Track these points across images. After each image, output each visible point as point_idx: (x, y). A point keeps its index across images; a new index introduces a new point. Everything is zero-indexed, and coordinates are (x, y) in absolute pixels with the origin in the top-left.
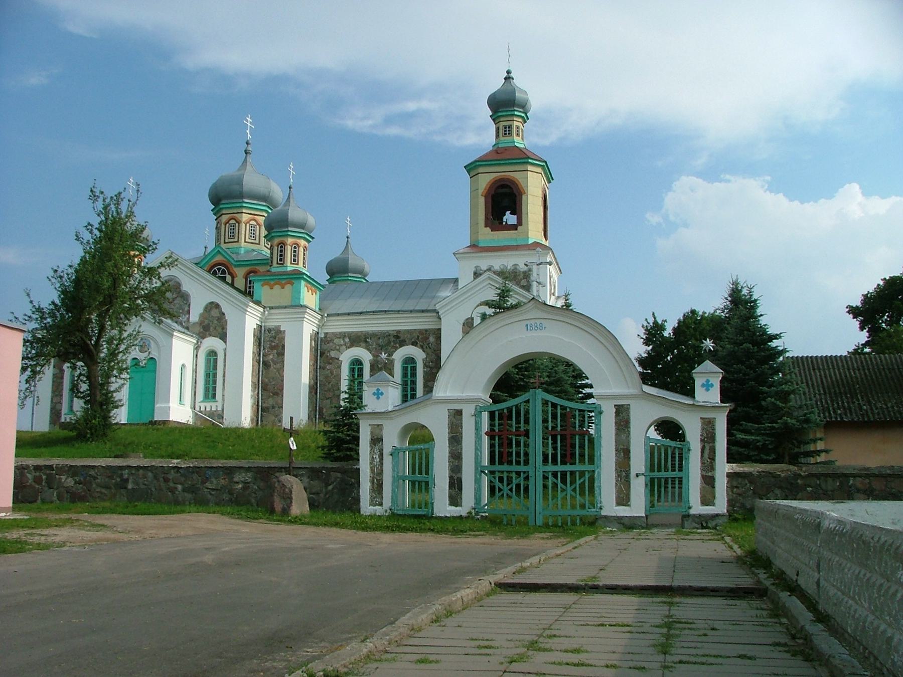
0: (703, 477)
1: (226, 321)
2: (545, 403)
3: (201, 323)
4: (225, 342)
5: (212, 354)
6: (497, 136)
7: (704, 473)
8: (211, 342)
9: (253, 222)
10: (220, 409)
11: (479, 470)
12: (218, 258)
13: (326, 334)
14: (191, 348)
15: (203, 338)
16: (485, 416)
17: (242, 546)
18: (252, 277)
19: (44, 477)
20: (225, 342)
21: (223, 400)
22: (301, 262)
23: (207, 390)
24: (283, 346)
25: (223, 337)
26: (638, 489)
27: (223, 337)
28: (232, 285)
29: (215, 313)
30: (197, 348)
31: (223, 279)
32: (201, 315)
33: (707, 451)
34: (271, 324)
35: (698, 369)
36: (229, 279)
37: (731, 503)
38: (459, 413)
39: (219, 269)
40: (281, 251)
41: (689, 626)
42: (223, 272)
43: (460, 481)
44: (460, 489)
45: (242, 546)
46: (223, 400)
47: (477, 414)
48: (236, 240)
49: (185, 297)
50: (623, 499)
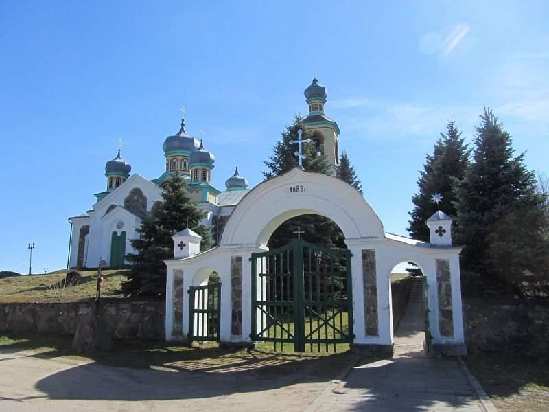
0: (441, 311)
6: (310, 111)
13: (221, 217)
33: (443, 288)
37: (467, 333)
38: (239, 259)
43: (240, 313)
44: (240, 320)
47: (253, 259)
49: (144, 199)
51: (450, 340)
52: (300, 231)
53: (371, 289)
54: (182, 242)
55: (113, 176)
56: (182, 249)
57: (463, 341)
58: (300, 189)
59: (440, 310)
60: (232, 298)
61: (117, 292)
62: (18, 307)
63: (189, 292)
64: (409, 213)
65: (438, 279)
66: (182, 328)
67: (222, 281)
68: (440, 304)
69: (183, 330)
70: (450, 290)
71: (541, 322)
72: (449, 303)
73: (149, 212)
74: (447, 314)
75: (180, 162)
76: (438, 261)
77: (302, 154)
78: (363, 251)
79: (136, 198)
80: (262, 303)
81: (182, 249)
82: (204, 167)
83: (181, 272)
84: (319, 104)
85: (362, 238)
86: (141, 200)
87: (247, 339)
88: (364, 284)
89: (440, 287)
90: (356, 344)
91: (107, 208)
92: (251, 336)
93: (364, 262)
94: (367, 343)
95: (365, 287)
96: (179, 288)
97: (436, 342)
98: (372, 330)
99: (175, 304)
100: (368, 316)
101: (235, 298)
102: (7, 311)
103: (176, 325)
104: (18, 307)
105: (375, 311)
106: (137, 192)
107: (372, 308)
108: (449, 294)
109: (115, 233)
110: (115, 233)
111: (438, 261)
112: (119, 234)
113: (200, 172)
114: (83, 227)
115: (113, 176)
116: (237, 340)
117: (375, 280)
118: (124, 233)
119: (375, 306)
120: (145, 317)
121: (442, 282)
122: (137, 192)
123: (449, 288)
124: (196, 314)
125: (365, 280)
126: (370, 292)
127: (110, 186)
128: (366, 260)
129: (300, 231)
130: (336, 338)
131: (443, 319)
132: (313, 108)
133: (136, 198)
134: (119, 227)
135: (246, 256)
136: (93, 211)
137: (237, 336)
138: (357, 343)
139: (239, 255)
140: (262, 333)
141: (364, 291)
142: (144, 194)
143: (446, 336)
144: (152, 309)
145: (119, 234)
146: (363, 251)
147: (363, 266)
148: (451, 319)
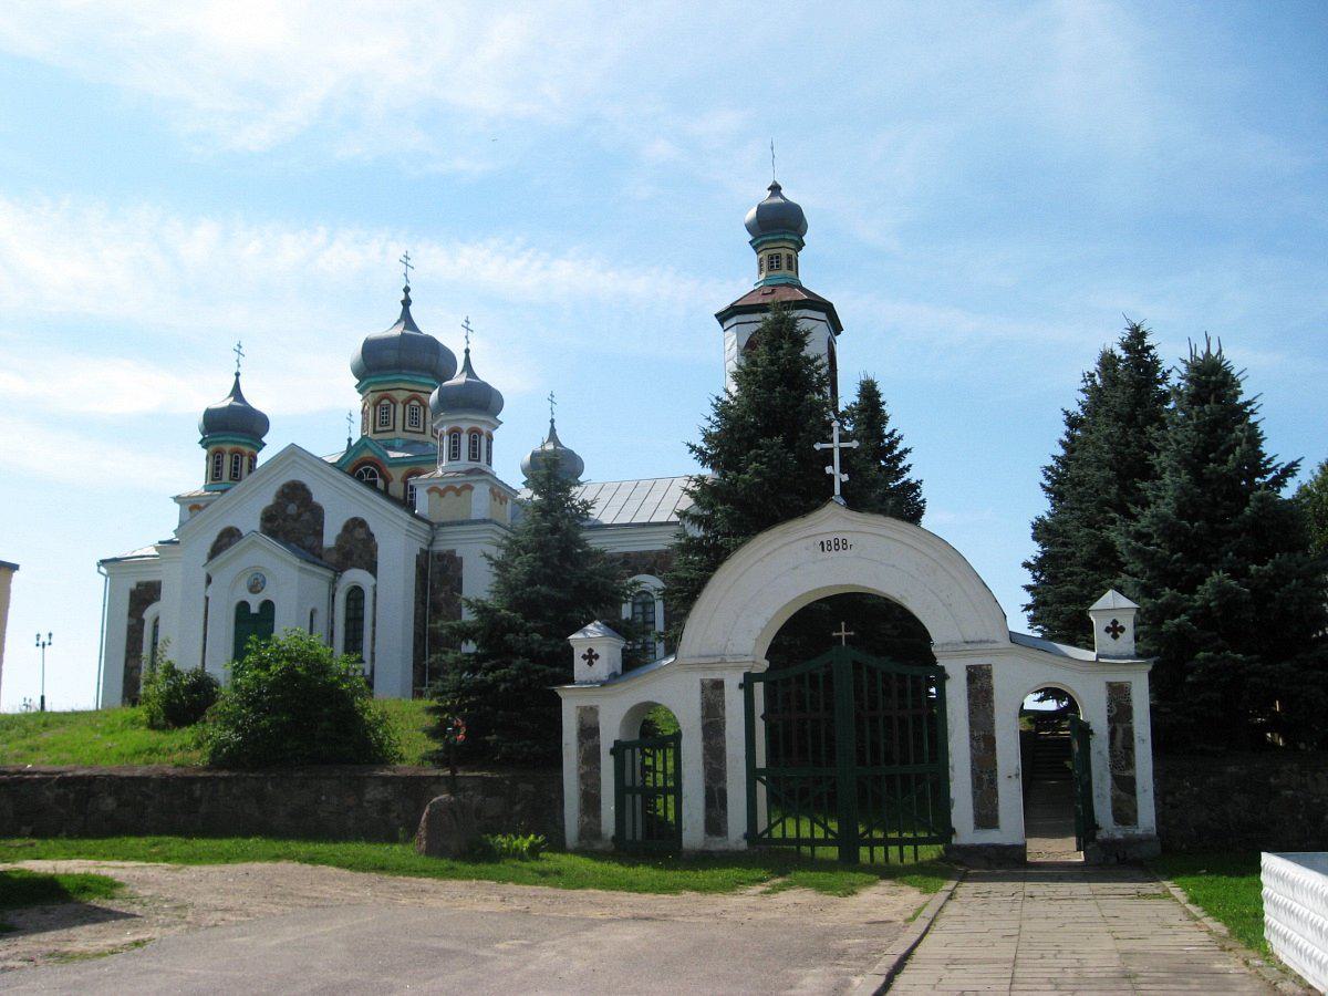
0: (1115, 778)
1: (376, 546)
2: (857, 666)
3: (339, 547)
4: (375, 576)
5: (356, 595)
7: (1117, 772)
8: (356, 576)
9: (385, 402)
10: (368, 672)
11: (753, 774)
12: (366, 454)
14: (325, 589)
15: (342, 571)
16: (759, 688)
17: (422, 380)
18: (412, 481)
19: (72, 796)
20: (375, 576)
21: (373, 660)
22: (484, 457)
23: (347, 641)
24: (460, 580)
25: (372, 568)
26: (1010, 794)
27: (372, 568)
28: (385, 494)
29: (359, 533)
30: (333, 584)
31: (372, 485)
32: (339, 538)
33: (1120, 735)
34: (442, 546)
35: (1098, 605)
36: (380, 483)
37: (1161, 817)
38: (718, 685)
39: (366, 470)
40: (455, 442)
41: (979, 976)
42: (373, 474)
43: (723, 794)
45: (422, 380)
46: (373, 660)
48: (391, 427)
49: (317, 513)
50: (986, 816)
51: (1130, 830)
52: (840, 637)
53: (984, 741)
54: (590, 651)
55: (242, 447)
56: (590, 664)
57: (1155, 832)
58: (840, 545)
59: (1113, 776)
60: (705, 764)
61: (199, 770)
62: (222, 786)
63: (612, 752)
64: (350, 440)
65: (1110, 720)
66: (600, 825)
67: (683, 727)
68: (1114, 766)
69: (603, 829)
70: (1132, 739)
71: (1291, 792)
72: (1130, 764)
73: (330, 550)
74: (1125, 785)
75: (400, 409)
76: (1110, 685)
77: (831, 477)
78: (968, 667)
79: (292, 509)
80: (761, 771)
81: (590, 664)
82: (452, 425)
83: (593, 711)
84: (784, 252)
85: (967, 642)
86: (307, 516)
87: (737, 842)
88: (971, 731)
89: (1113, 734)
90: (958, 846)
91: (212, 536)
92: (746, 836)
93: (969, 690)
94: (978, 842)
95: (972, 738)
96: (590, 743)
97: (1106, 836)
98: (986, 816)
99: (582, 777)
100: (979, 792)
101: (711, 763)
102: (198, 793)
103: (586, 820)
104: (222, 786)
105: (993, 782)
106: (295, 493)
107: (986, 777)
108: (1129, 748)
109: (243, 607)
110: (243, 607)
111: (1110, 685)
112: (254, 609)
113: (227, 459)
114: (139, 585)
115: (242, 447)
116: (717, 844)
117: (992, 724)
118: (268, 607)
119: (993, 772)
120: (515, 804)
121: (1117, 724)
122: (295, 493)
123: (1129, 734)
124: (629, 797)
125: (973, 725)
126: (982, 746)
127: (215, 473)
128: (974, 686)
129: (840, 637)
130: (912, 847)
131: (1119, 792)
132: (773, 263)
133: (292, 509)
134: (255, 588)
135: (732, 681)
136: (178, 542)
137: (718, 839)
138: (959, 843)
139: (717, 676)
140: (769, 830)
141: (971, 746)
142: (315, 499)
143: (1124, 824)
144: (531, 788)
145: (254, 609)
146: (968, 667)
147: (969, 697)
148: (1133, 793)
